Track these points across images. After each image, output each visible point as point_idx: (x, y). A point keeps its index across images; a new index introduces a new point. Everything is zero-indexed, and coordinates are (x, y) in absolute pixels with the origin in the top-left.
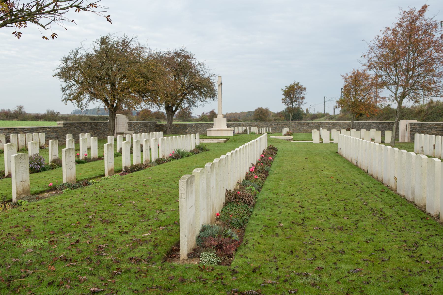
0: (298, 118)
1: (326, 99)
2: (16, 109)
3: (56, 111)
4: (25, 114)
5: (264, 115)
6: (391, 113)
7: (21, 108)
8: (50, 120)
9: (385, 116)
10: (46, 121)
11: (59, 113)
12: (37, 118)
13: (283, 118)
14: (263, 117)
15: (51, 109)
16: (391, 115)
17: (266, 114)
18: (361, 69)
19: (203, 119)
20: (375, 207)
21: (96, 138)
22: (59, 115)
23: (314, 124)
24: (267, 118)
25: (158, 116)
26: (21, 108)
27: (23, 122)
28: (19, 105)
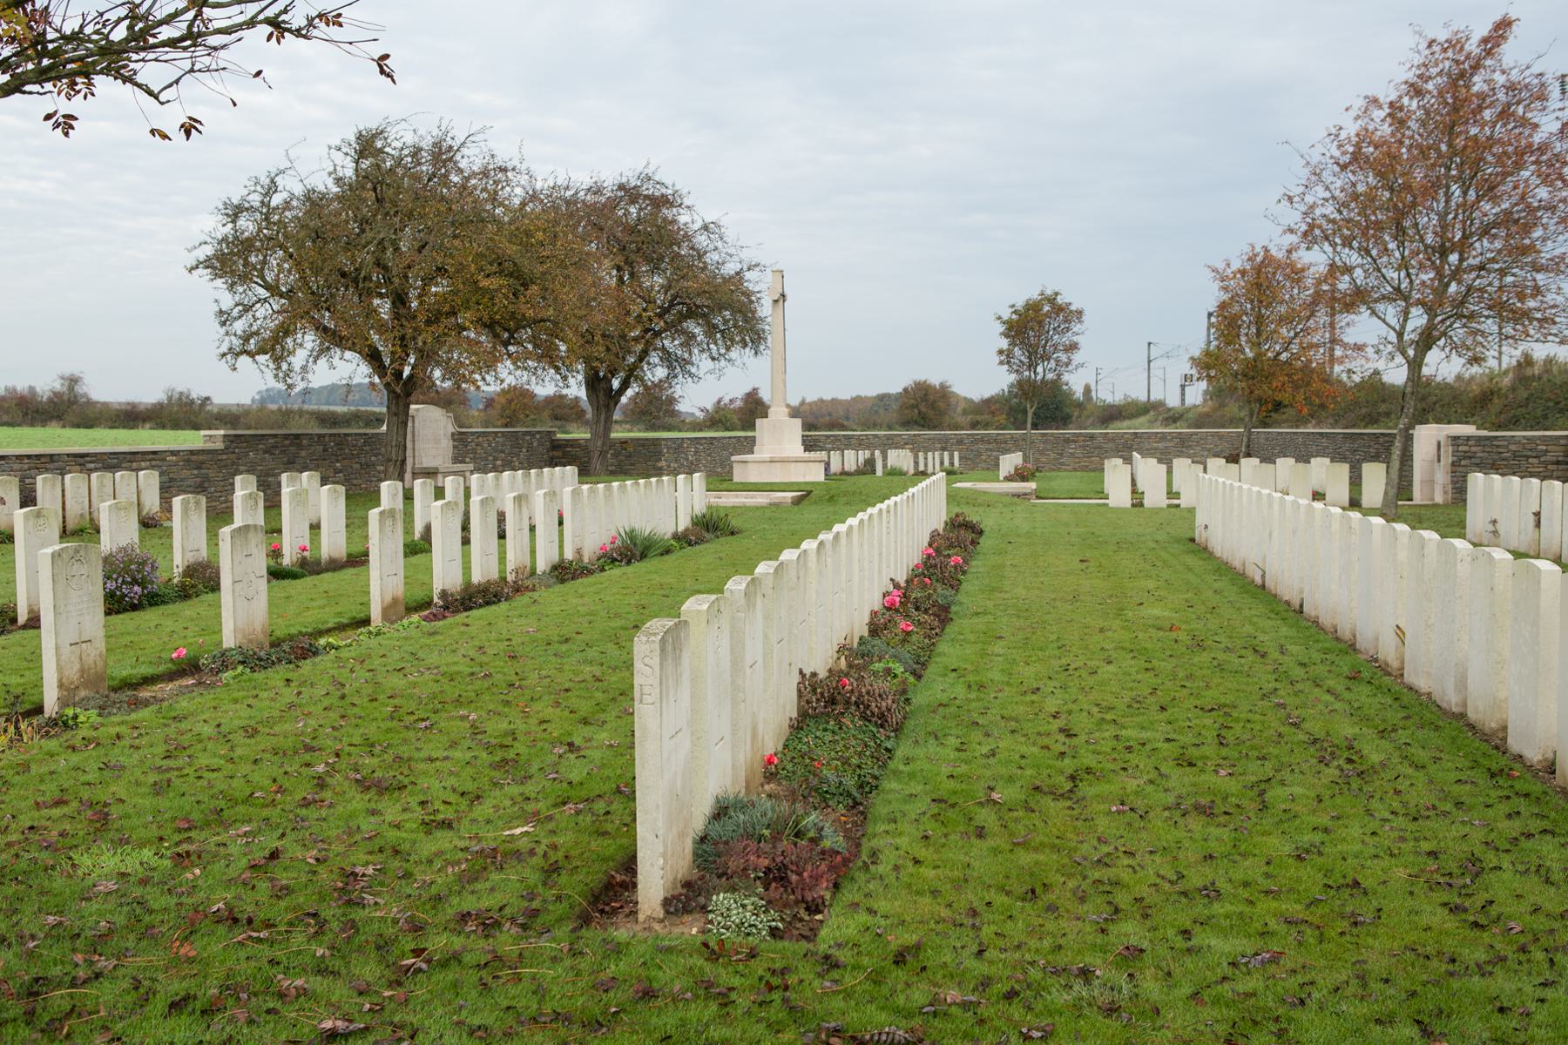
0: (1054, 419)
1: (1154, 352)
2: (58, 386)
3: (197, 393)
4: (90, 403)
5: (933, 406)
6: (1384, 401)
7: (73, 381)
8: (176, 425)
9: (1364, 411)
10: (164, 427)
11: (208, 399)
12: (131, 417)
13: (1002, 418)
14: (931, 413)
15: (181, 387)
16: (1383, 408)
17: (941, 405)
18: (1278, 245)
19: (720, 421)
20: (1328, 734)
21: (341, 489)
22: (209, 408)
23: (1113, 440)
24: (947, 420)
25: (559, 411)
26: (73, 381)
27: (83, 431)
28: (67, 373)
